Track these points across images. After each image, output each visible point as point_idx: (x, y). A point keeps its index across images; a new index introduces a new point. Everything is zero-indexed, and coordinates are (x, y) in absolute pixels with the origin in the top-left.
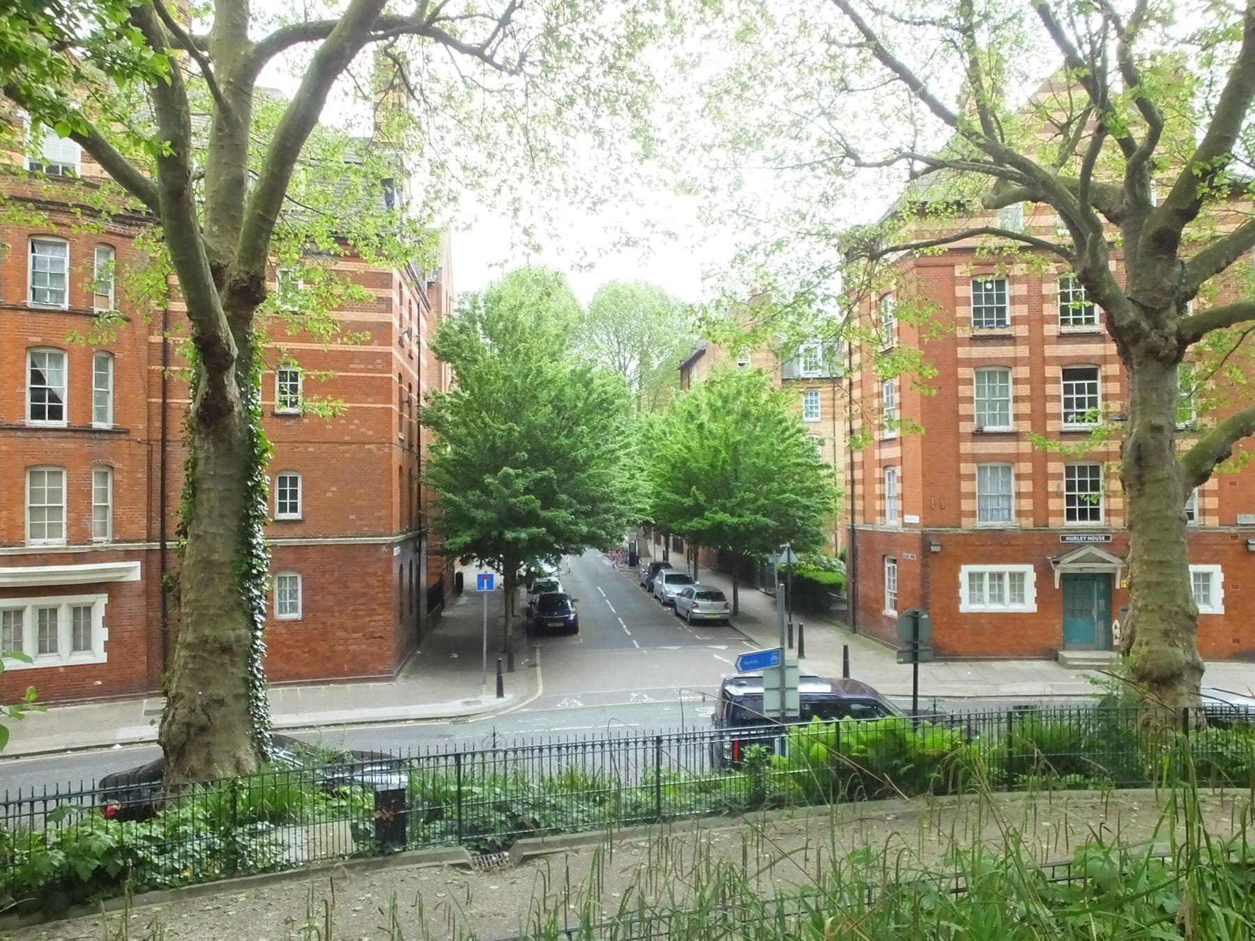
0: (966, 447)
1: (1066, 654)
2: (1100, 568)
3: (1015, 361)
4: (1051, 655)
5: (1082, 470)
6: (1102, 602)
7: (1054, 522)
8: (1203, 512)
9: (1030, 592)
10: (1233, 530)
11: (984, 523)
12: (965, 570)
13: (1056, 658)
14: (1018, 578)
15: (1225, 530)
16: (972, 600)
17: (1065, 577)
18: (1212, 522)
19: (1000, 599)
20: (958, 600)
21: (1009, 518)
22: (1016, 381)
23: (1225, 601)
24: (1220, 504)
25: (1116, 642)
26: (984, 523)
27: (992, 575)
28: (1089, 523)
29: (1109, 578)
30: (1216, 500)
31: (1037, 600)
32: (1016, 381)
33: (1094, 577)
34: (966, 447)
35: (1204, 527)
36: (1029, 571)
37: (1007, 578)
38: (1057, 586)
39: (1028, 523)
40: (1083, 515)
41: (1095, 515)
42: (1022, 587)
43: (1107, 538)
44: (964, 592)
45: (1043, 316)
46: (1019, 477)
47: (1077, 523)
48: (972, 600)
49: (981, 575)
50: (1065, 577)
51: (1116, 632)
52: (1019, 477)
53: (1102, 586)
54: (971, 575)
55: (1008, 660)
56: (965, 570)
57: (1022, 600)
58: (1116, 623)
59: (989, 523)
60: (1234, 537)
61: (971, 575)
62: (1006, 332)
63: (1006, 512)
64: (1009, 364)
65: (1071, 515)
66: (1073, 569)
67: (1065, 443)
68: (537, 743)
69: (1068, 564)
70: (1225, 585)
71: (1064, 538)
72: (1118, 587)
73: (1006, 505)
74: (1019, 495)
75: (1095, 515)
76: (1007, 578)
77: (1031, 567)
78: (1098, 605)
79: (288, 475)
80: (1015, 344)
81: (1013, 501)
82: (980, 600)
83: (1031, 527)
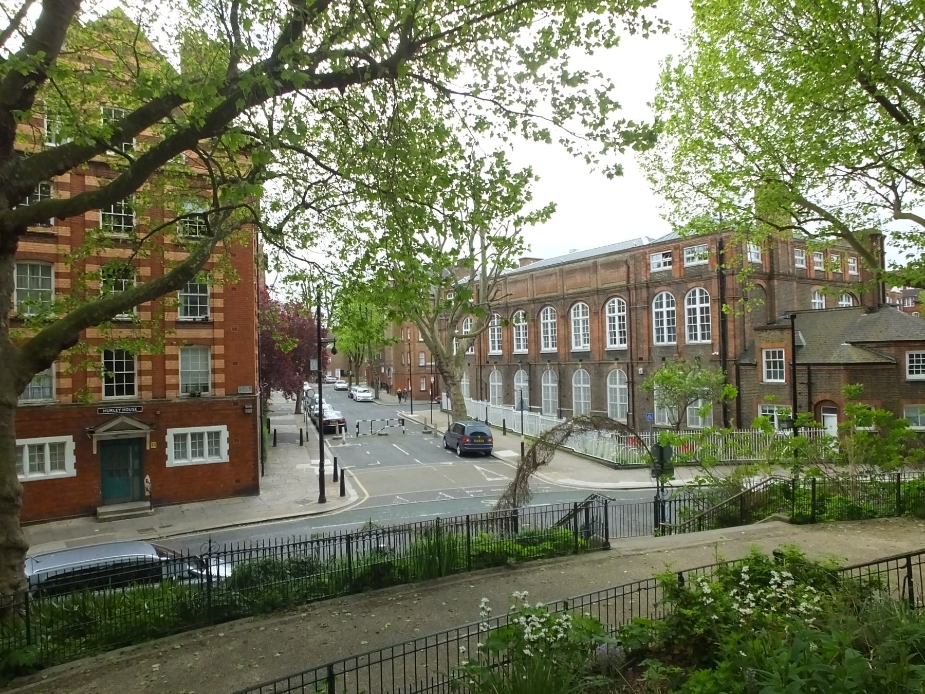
0: (219, 333)
1: (100, 510)
2: (133, 434)
3: (57, 258)
4: (90, 512)
5: (119, 354)
6: (137, 462)
7: (92, 399)
8: (214, 385)
9: (70, 459)
10: (235, 398)
11: (25, 401)
12: (171, 432)
13: (95, 514)
14: (57, 449)
15: (229, 398)
16: (177, 457)
17: (102, 444)
18: (221, 392)
19: (41, 468)
20: (166, 457)
21: (51, 396)
22: (58, 275)
23: (229, 452)
24: (226, 379)
25: (147, 494)
26: (25, 401)
27: (193, 435)
28: (125, 397)
29: (141, 441)
30: (223, 376)
31: (76, 466)
32: (58, 275)
33: (130, 441)
34: (219, 333)
35: (214, 397)
36: (69, 441)
37: (47, 450)
38: (95, 452)
39: (67, 399)
40: (120, 391)
41: (130, 390)
42: (218, 443)
43: (139, 409)
44: (170, 451)
45: (85, 221)
46: (214, 357)
47: (115, 397)
48: (177, 457)
49: (184, 436)
50: (102, 444)
51: (147, 485)
52: (214, 357)
53: (136, 448)
54: (176, 437)
55: (49, 521)
56: (171, 432)
57: (62, 467)
58: (147, 477)
59: (30, 401)
60: (236, 403)
61: (176, 437)
62: (49, 231)
63: (47, 391)
64: (52, 259)
65: (109, 392)
66: (110, 436)
67: (178, 331)
68: (332, 535)
69: (103, 433)
70: (229, 440)
71: (101, 411)
72: (148, 448)
73: (47, 384)
74: (214, 371)
75: (130, 390)
76: (47, 450)
77: (225, 426)
78: (133, 463)
79: (777, 350)
80: (57, 243)
81: (54, 380)
82: (184, 456)
83: (71, 403)
